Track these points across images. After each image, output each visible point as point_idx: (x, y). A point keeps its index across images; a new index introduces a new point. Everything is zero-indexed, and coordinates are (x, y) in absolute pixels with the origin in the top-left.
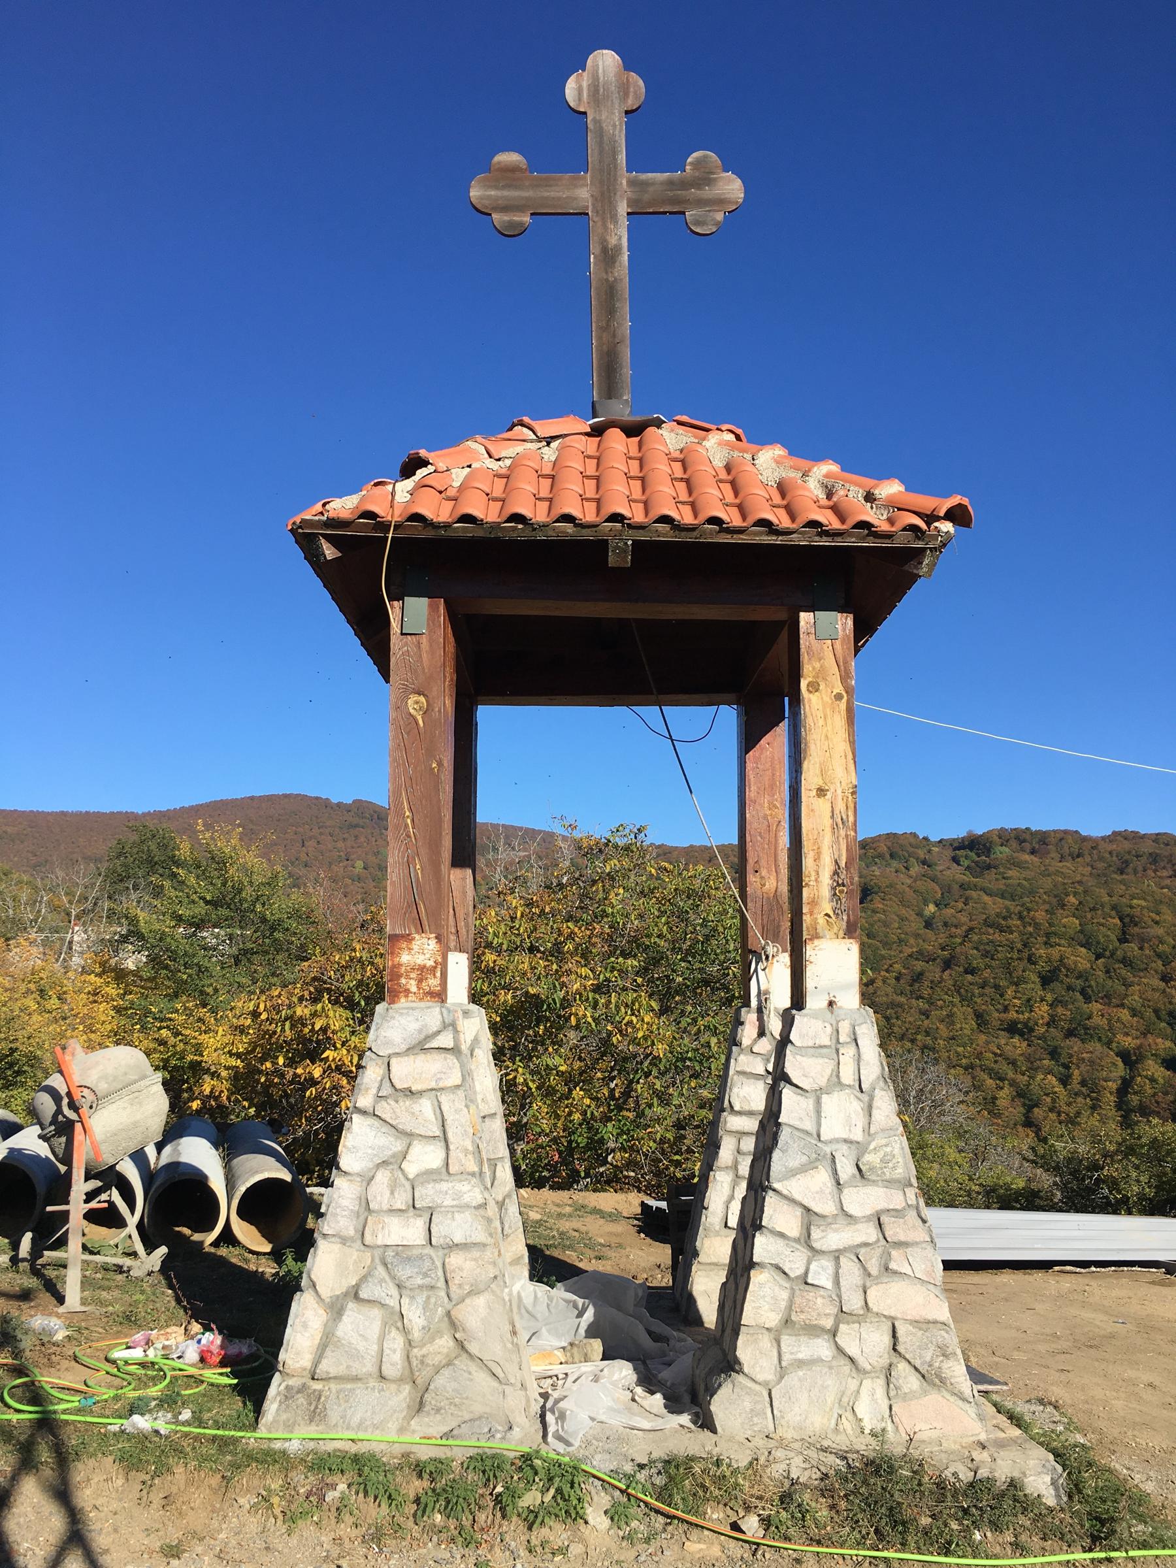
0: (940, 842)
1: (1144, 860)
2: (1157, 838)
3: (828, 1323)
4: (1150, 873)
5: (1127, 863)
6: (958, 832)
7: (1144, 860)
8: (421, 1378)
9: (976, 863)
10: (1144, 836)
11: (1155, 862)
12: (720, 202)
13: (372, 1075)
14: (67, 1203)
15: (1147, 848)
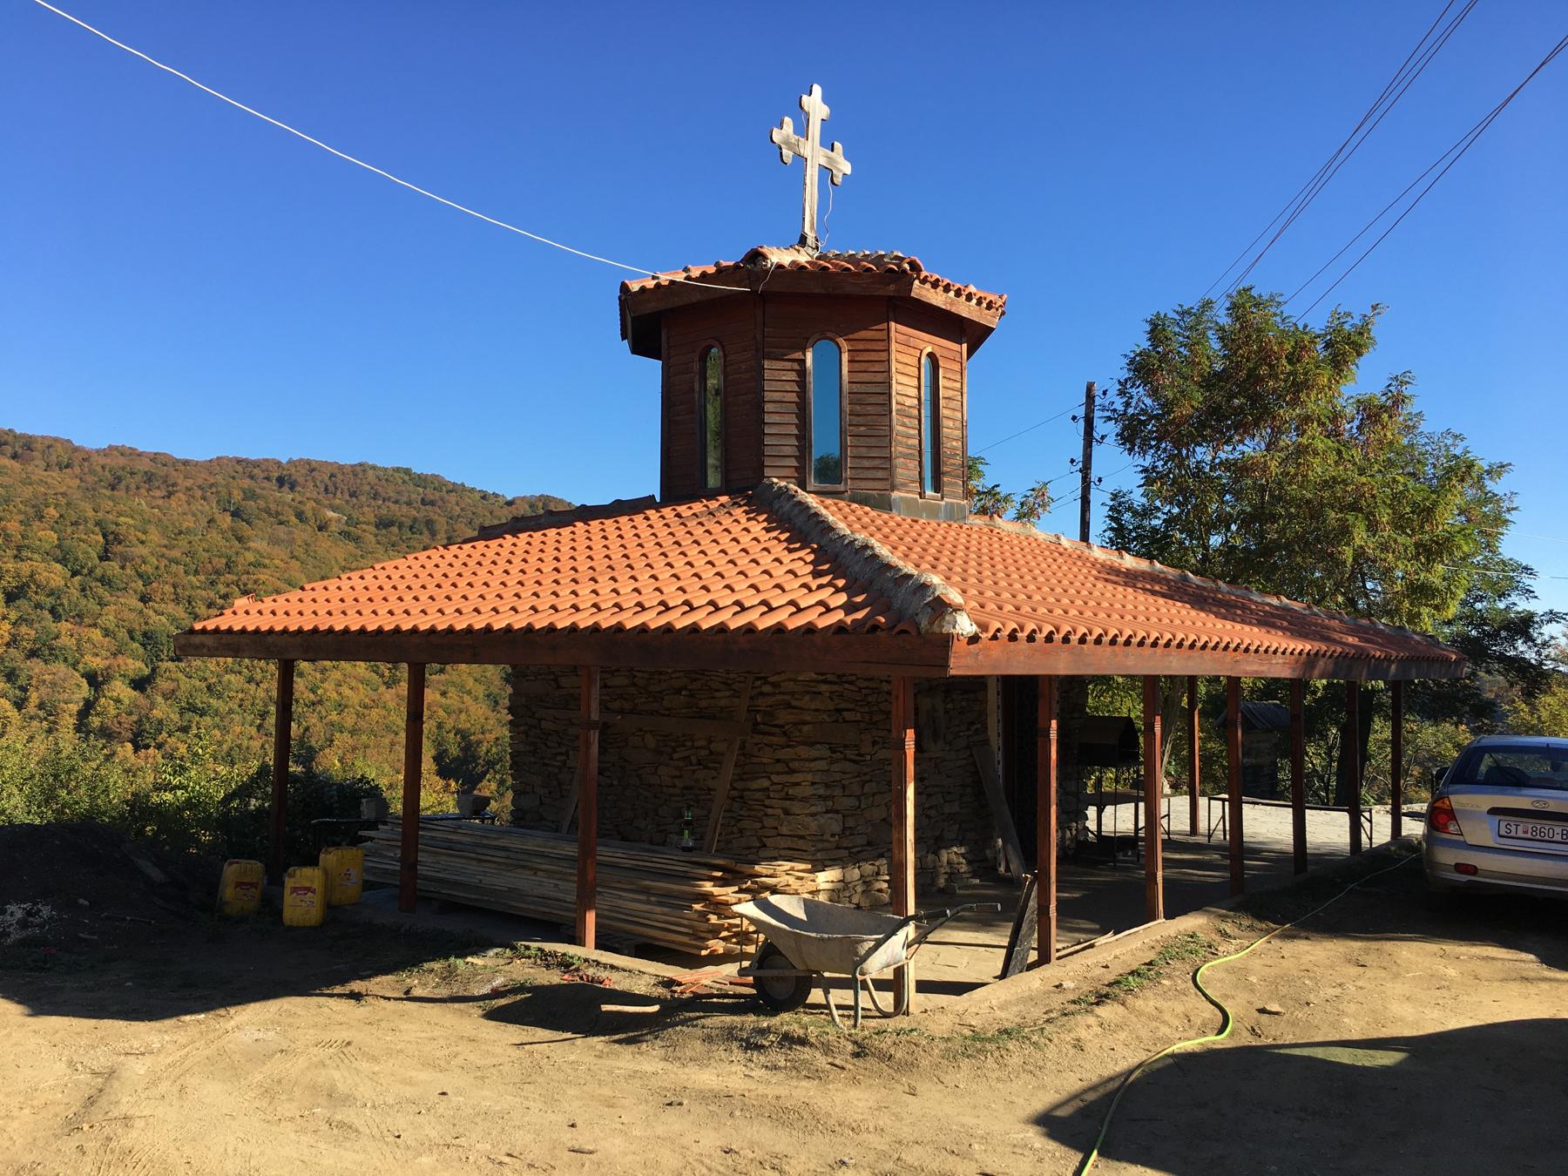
2: (155, 458)
4: (143, 491)
5: (119, 479)
7: (138, 478)
11: (150, 480)
15: (143, 466)
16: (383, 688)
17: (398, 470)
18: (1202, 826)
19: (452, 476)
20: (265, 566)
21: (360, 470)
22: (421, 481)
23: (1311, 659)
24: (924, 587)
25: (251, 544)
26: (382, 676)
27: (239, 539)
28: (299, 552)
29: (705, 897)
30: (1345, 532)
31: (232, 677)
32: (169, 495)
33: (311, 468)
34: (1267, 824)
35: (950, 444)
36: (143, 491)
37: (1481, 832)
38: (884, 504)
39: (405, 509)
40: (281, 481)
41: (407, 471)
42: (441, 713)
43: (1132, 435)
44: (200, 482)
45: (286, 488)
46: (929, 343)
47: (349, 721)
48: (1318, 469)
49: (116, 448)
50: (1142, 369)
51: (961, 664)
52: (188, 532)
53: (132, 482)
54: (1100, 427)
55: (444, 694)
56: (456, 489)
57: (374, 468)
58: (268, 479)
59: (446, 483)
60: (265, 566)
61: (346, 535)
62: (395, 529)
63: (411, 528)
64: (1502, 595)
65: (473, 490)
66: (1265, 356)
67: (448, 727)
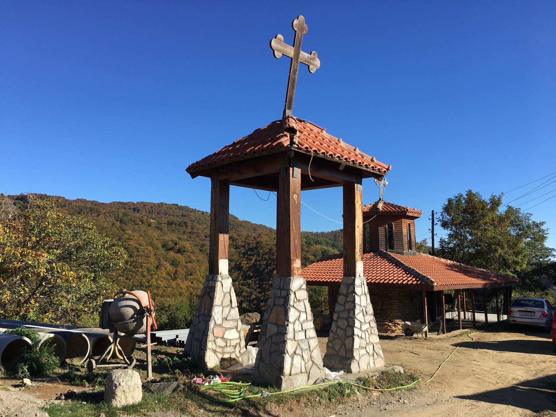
0: (8, 196)
1: (88, 210)
2: (92, 202)
3: (365, 346)
4: (89, 214)
5: (81, 210)
6: (17, 193)
7: (88, 210)
8: (308, 371)
9: (23, 206)
10: (106, 204)
11: (91, 210)
12: (316, 66)
13: (292, 297)
14: (147, 344)
15: (89, 205)
16: (171, 281)
17: (173, 205)
18: (467, 318)
19: (192, 206)
20: (132, 239)
21: (161, 205)
22: (181, 208)
23: (486, 284)
24: (428, 279)
25: (127, 232)
26: (171, 277)
27: (123, 230)
28: (143, 234)
29: (386, 325)
30: (496, 250)
31: (121, 278)
32: (98, 215)
33: (144, 204)
34: (480, 317)
35: (413, 240)
36: (89, 214)
37: (517, 315)
38: (402, 254)
39: (176, 218)
40: (134, 209)
41: (177, 205)
42: (192, 290)
43: (445, 225)
44: (108, 210)
45: (136, 212)
46: (408, 221)
47: (161, 292)
48: (489, 234)
49: (80, 199)
50: (447, 209)
51: (435, 289)
52: (106, 228)
53: (86, 211)
54: (436, 222)
55: (192, 283)
56: (194, 211)
57: (165, 204)
58: (130, 209)
59: (190, 209)
60: (132, 239)
61: (157, 228)
62: (174, 225)
63: (179, 225)
64: (547, 256)
65: (199, 211)
66: (475, 208)
67: (194, 294)
